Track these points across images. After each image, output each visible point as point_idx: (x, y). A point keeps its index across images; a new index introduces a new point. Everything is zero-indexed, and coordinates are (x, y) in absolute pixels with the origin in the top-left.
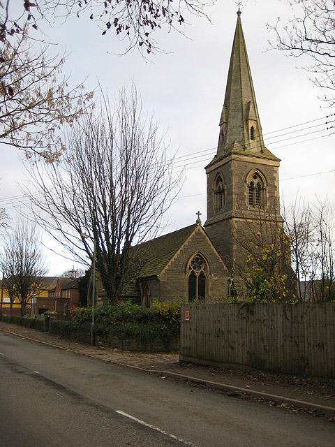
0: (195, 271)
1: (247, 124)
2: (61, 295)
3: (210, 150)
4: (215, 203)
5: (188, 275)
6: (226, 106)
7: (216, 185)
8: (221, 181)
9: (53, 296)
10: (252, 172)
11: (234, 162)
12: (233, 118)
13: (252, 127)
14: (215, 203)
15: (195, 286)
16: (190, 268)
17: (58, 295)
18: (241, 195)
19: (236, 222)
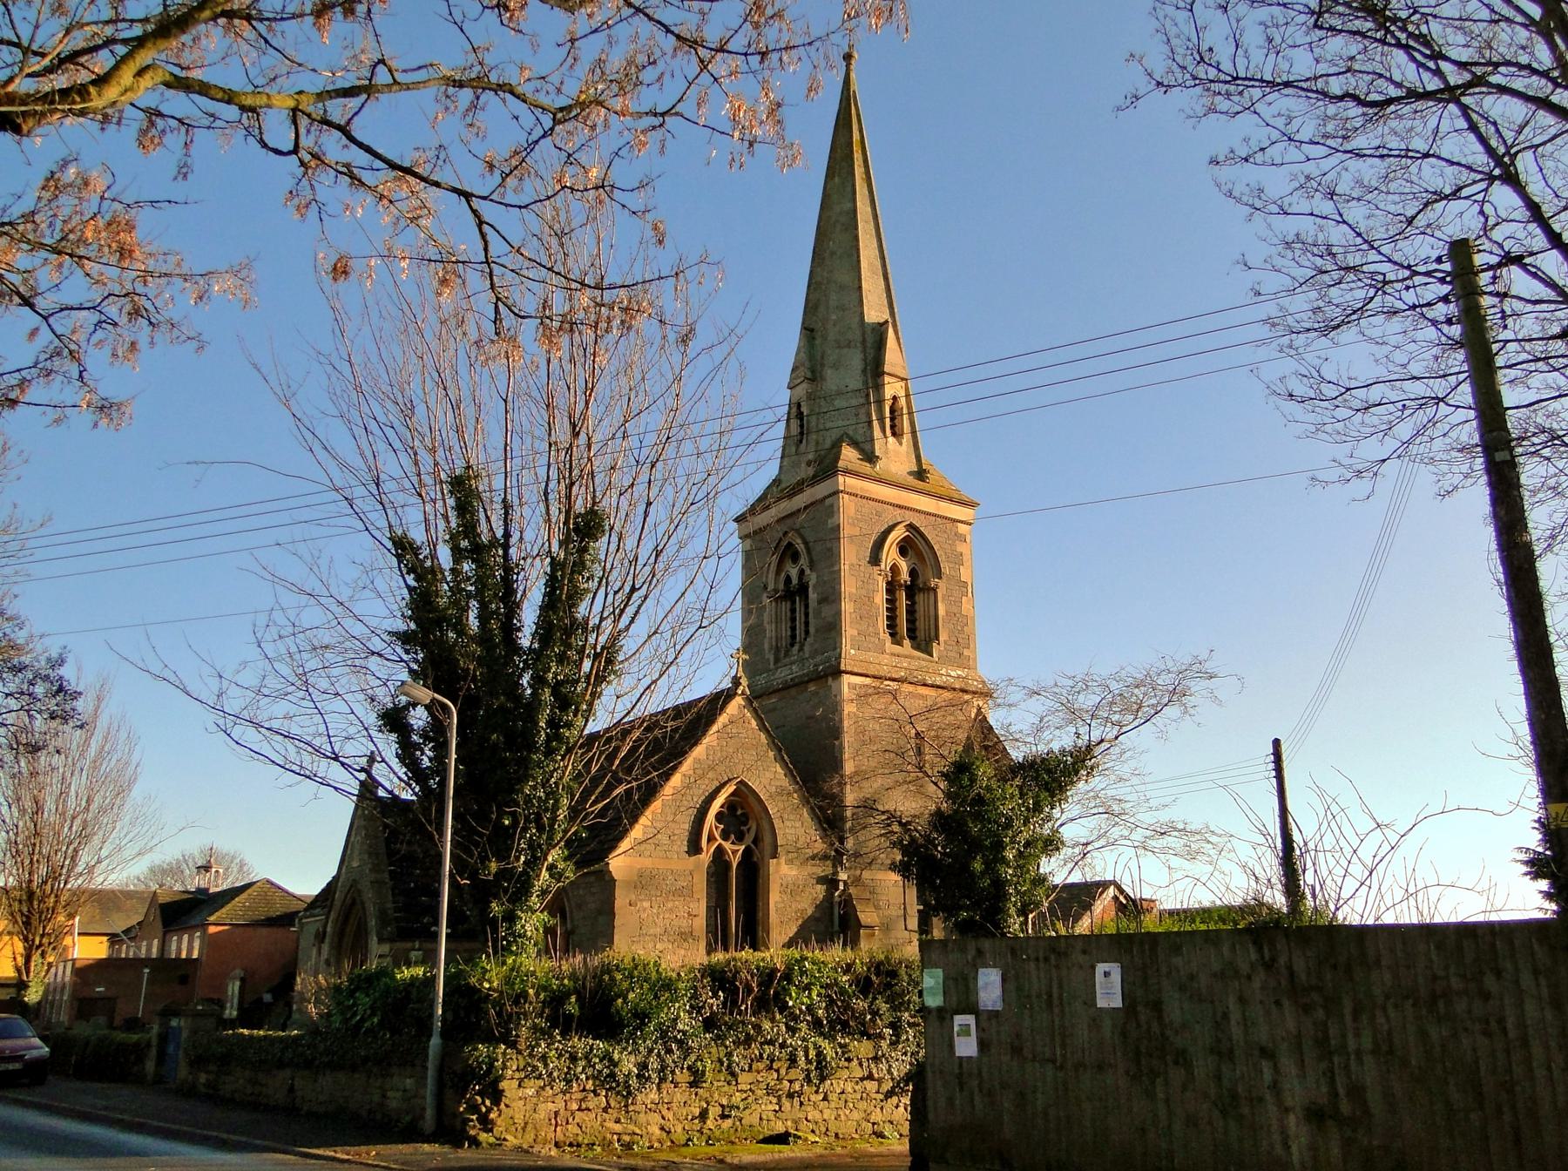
0: (727, 846)
1: (879, 387)
2: (163, 947)
3: (759, 467)
4: (770, 629)
5: (705, 858)
6: (808, 331)
7: (778, 573)
8: (795, 557)
9: (125, 952)
10: (898, 534)
11: (844, 500)
12: (836, 366)
13: (895, 398)
14: (770, 629)
15: (438, 878)
16: (711, 839)
17: (150, 948)
18: (866, 600)
19: (852, 687)
